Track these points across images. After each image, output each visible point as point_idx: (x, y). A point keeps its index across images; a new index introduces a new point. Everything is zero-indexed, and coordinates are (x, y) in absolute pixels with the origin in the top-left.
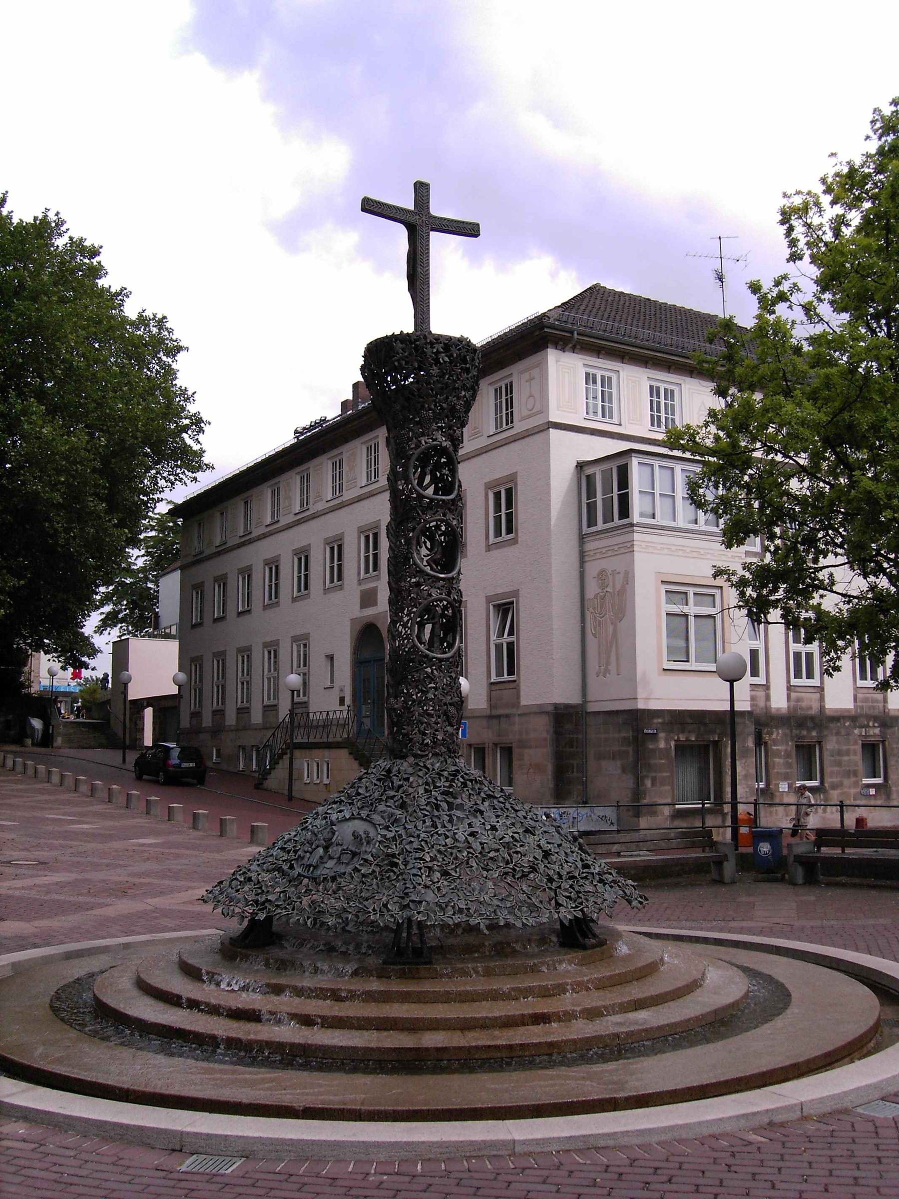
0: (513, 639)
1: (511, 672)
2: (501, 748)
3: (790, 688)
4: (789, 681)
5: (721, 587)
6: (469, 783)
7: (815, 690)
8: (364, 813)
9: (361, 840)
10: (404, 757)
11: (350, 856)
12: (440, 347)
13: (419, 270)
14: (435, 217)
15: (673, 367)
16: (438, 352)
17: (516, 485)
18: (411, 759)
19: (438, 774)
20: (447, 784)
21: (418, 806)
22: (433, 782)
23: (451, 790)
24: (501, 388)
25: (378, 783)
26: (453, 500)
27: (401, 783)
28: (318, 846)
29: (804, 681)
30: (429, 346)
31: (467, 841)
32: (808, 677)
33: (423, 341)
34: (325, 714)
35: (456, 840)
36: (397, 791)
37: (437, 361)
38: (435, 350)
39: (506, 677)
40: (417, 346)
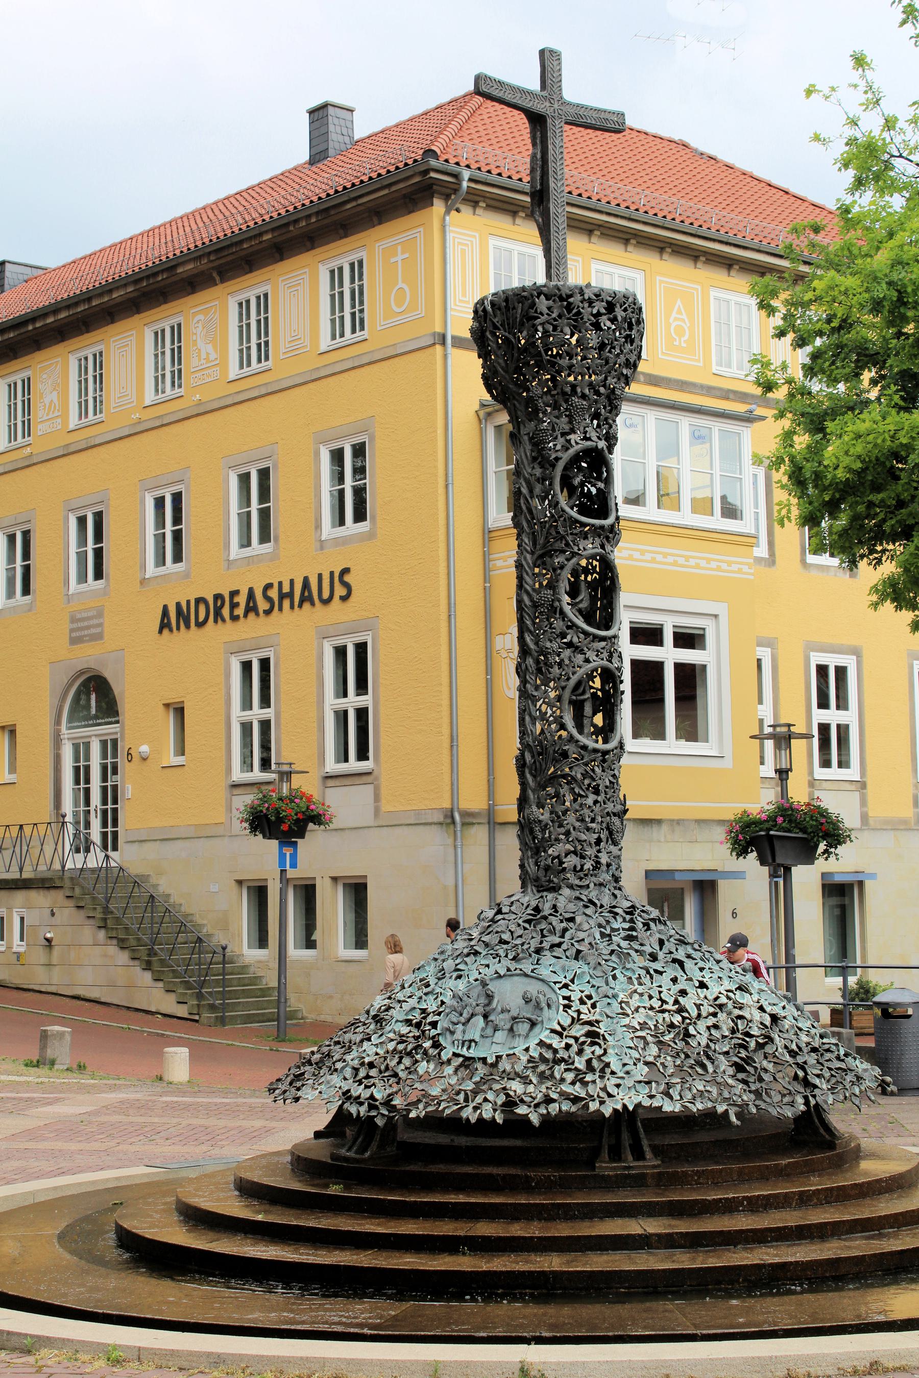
0: (365, 701)
1: (363, 755)
2: (295, 886)
3: (812, 783)
4: (811, 772)
5: (716, 616)
6: (652, 924)
7: (853, 787)
8: (527, 966)
9: (538, 1003)
10: (555, 889)
11: (527, 1026)
12: (599, 307)
13: (552, 185)
14: (569, 104)
15: (633, 241)
16: (599, 314)
17: (372, 438)
18: (566, 891)
19: (610, 912)
20: (627, 925)
21: (600, 955)
22: (608, 922)
23: (634, 934)
24: (341, 269)
25: (527, 926)
26: (613, 526)
27: (564, 925)
28: (473, 1015)
29: (834, 772)
30: (586, 305)
31: (676, 1002)
32: (840, 765)
33: (579, 298)
34: (15, 831)
35: (664, 1002)
36: (562, 936)
37: (597, 326)
38: (595, 311)
39: (354, 765)
40: (570, 304)
